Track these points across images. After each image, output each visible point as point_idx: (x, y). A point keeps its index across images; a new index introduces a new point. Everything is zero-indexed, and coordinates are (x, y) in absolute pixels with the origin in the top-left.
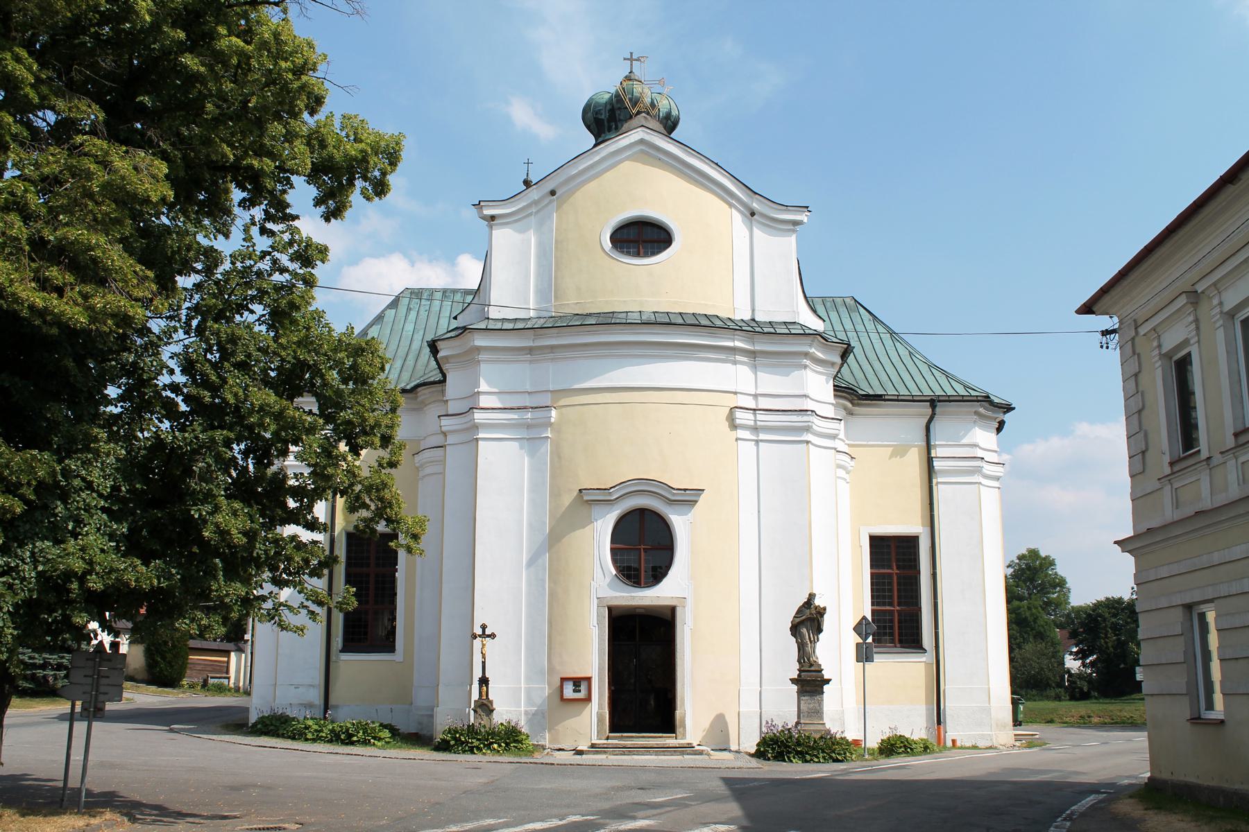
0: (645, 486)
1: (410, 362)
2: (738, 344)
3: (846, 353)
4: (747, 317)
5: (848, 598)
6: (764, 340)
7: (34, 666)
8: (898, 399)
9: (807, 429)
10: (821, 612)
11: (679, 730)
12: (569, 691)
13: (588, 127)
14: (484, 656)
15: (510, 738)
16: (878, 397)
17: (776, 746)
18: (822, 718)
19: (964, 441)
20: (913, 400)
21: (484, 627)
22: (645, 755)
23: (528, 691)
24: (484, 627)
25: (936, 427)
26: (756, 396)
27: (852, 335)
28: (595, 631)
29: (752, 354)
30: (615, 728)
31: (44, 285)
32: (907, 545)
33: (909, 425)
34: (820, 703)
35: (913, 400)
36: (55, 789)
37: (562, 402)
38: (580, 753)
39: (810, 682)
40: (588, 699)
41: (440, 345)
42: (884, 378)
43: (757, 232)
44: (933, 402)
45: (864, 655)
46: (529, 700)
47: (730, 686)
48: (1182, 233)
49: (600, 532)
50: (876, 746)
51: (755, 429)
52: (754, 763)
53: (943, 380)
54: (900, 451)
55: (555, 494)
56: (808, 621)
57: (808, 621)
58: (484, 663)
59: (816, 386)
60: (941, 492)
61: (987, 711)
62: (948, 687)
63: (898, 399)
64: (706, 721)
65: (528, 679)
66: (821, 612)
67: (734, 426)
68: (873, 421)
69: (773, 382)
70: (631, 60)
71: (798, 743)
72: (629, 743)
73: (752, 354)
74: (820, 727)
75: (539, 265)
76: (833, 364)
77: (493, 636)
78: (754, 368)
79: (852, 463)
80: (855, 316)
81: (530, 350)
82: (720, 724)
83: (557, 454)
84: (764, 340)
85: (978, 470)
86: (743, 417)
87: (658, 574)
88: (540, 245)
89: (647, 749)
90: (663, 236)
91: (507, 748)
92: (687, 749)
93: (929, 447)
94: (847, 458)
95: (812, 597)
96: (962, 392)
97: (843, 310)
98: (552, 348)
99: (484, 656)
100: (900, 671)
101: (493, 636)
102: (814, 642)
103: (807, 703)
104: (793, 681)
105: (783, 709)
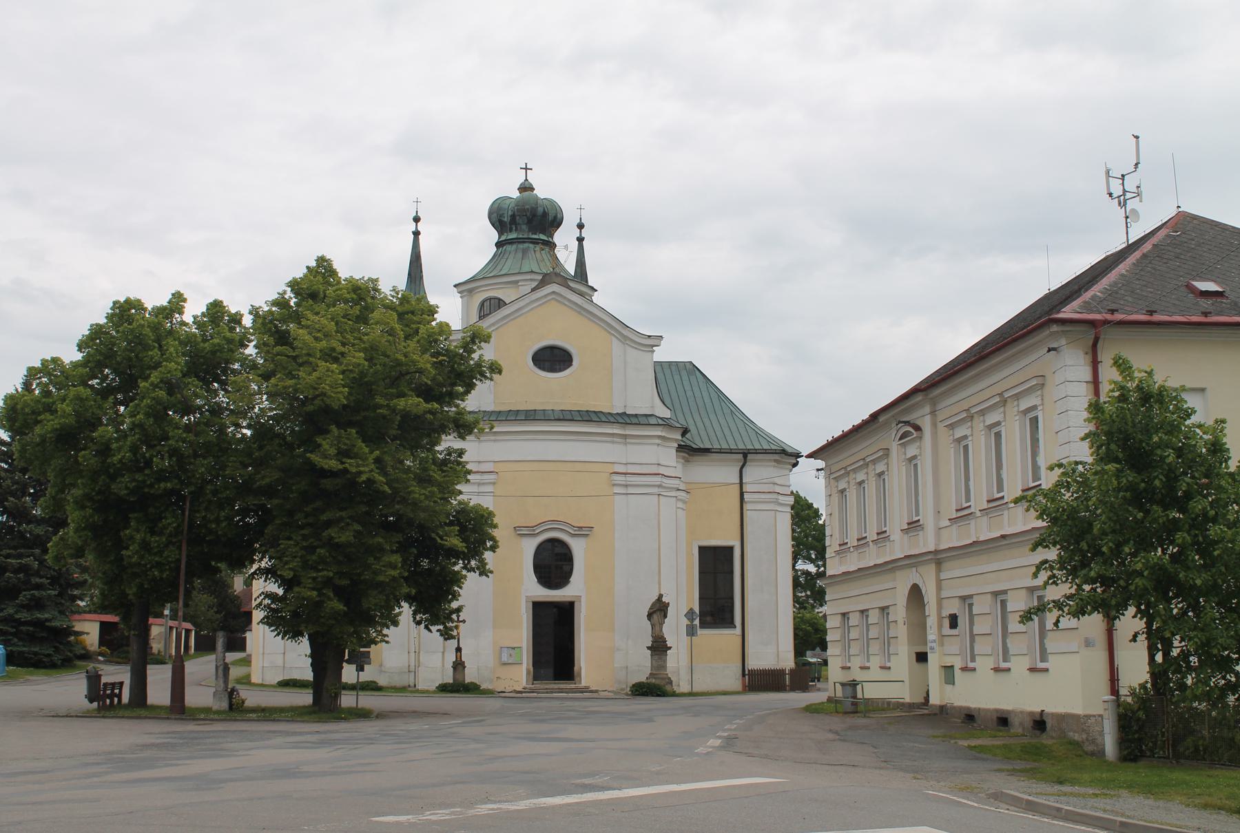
0: (555, 524)
2: (616, 431)
3: (685, 432)
5: (684, 594)
8: (720, 451)
11: (577, 679)
16: (707, 451)
20: (731, 452)
25: (746, 470)
27: (691, 422)
34: (665, 661)
35: (731, 452)
39: (659, 647)
43: (630, 350)
45: (691, 632)
47: (607, 649)
56: (659, 609)
57: (659, 609)
59: (667, 457)
62: (749, 651)
63: (720, 451)
70: (526, 169)
72: (562, 686)
77: (464, 621)
80: (693, 378)
89: (561, 691)
94: (683, 494)
95: (661, 596)
97: (684, 373)
100: (721, 639)
102: (661, 624)
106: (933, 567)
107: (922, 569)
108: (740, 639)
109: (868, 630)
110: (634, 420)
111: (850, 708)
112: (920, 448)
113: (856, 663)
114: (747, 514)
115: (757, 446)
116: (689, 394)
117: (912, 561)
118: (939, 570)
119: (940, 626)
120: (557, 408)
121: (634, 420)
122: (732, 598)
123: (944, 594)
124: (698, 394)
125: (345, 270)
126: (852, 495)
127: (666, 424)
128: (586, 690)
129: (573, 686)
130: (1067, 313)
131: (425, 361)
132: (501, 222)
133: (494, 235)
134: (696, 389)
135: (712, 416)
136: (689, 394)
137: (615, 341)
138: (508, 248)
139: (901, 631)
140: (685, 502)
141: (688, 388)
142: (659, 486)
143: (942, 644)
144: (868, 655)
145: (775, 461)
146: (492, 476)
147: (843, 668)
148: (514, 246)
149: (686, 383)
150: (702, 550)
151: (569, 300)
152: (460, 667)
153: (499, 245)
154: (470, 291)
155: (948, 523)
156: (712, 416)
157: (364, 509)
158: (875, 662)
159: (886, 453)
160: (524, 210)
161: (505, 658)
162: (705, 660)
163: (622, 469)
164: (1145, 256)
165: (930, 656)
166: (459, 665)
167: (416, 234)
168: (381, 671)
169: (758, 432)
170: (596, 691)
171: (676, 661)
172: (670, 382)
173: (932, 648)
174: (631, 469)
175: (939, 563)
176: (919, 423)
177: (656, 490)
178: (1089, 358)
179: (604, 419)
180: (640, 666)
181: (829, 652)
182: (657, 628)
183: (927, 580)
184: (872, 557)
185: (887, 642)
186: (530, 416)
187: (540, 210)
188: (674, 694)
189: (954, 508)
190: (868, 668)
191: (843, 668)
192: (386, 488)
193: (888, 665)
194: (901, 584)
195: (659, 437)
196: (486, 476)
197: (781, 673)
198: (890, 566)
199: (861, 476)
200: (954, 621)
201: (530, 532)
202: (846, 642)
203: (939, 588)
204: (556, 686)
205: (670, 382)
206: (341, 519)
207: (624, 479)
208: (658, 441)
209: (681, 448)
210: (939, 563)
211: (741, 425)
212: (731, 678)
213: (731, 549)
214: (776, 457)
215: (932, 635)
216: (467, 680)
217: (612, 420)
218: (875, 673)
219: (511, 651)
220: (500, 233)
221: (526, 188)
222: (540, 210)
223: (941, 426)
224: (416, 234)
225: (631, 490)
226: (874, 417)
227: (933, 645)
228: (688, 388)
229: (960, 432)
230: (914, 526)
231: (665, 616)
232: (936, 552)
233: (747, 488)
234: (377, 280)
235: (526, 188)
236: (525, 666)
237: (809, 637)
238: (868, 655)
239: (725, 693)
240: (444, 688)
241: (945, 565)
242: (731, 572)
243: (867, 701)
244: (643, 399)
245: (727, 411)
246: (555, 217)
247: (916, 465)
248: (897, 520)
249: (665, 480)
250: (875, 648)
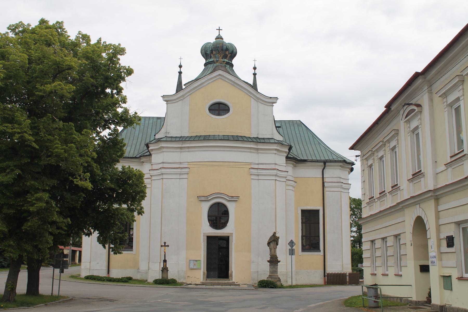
1: (138, 147)
2: (252, 146)
3: (290, 148)
5: (292, 231)
11: (230, 278)
13: (203, 56)
14: (165, 253)
16: (305, 161)
18: (277, 274)
20: (317, 161)
21: (165, 243)
24: (165, 243)
28: (203, 244)
30: (208, 277)
34: (277, 268)
35: (317, 161)
36: (49, 296)
39: (274, 261)
41: (150, 145)
42: (308, 152)
43: (260, 104)
44: (325, 162)
45: (292, 252)
47: (246, 263)
48: (381, 125)
50: (83, 277)
53: (329, 154)
58: (165, 255)
59: (281, 160)
70: (219, 30)
74: (276, 277)
76: (286, 152)
77: (168, 246)
79: (296, 184)
80: (300, 128)
81: (181, 148)
87: (223, 225)
89: (219, 284)
90: (227, 108)
94: (293, 183)
95: (275, 233)
98: (188, 147)
99: (165, 253)
100: (316, 256)
101: (168, 246)
102: (275, 248)
104: (268, 261)
106: (432, 202)
107: (424, 205)
108: (323, 257)
109: (387, 251)
110: (262, 141)
111: (373, 304)
112: (420, 119)
113: (380, 271)
114: (326, 193)
115: (331, 158)
116: (298, 135)
117: (416, 200)
118: (437, 204)
119: (439, 246)
120: (221, 134)
121: (262, 141)
122: (319, 236)
123: (441, 222)
124: (302, 135)
126: (376, 167)
127: (279, 143)
128: (233, 284)
129: (226, 282)
131: (75, 62)
132: (206, 54)
133: (203, 61)
135: (309, 145)
136: (298, 135)
137: (252, 100)
138: (209, 66)
139: (409, 250)
140: (294, 187)
141: (297, 132)
142: (276, 175)
143: (441, 259)
144: (387, 267)
145: (341, 166)
146: (187, 170)
147: (383, 275)
148: (212, 65)
149: (297, 130)
150: (303, 211)
151: (228, 79)
152: (165, 271)
153: (206, 65)
155: (444, 168)
156: (309, 145)
157: (28, 160)
158: (391, 271)
159: (397, 132)
160: (217, 47)
161: (192, 266)
162: (298, 268)
163: (256, 166)
165: (431, 268)
166: (165, 270)
167: (180, 73)
168: (138, 272)
169: (332, 152)
170: (239, 285)
171: (282, 269)
172: (289, 130)
173: (433, 262)
174: (261, 166)
175: (437, 199)
176: (419, 103)
177: (274, 178)
179: (245, 140)
180: (264, 271)
181: (364, 264)
182: (273, 251)
183: (428, 212)
184: (389, 202)
185: (400, 258)
186: (206, 138)
187: (225, 47)
188: (282, 287)
189: (449, 155)
190: (387, 275)
191: (383, 275)
192: (34, 145)
193: (400, 273)
194: (409, 218)
195: (276, 150)
196: (184, 170)
197: (344, 275)
198: (401, 206)
199: (381, 154)
200: (450, 242)
201: (202, 199)
202: (373, 259)
203: (438, 217)
204: (217, 282)
205: (289, 130)
206: (8, 167)
207: (256, 171)
208: (275, 152)
209: (287, 158)
210: (437, 199)
211: (323, 149)
212: (318, 278)
213: (318, 211)
214: (341, 164)
215: (433, 252)
216: (169, 278)
217: (250, 140)
218: (392, 279)
219: (195, 262)
221: (219, 38)
222: (225, 47)
223: (436, 98)
224: (180, 73)
225: (260, 177)
226: (388, 106)
227: (433, 259)
228: (297, 132)
229: (451, 98)
231: (277, 244)
232: (435, 190)
233: (326, 180)
234: (62, 22)
235: (219, 38)
236: (202, 270)
237: (357, 258)
238: (387, 267)
239: (311, 286)
240: (157, 282)
241: (441, 201)
242: (318, 223)
243: (387, 298)
244: (268, 131)
245: (316, 142)
246: (233, 52)
247: (418, 135)
248: (406, 172)
249: (279, 172)
250: (391, 262)
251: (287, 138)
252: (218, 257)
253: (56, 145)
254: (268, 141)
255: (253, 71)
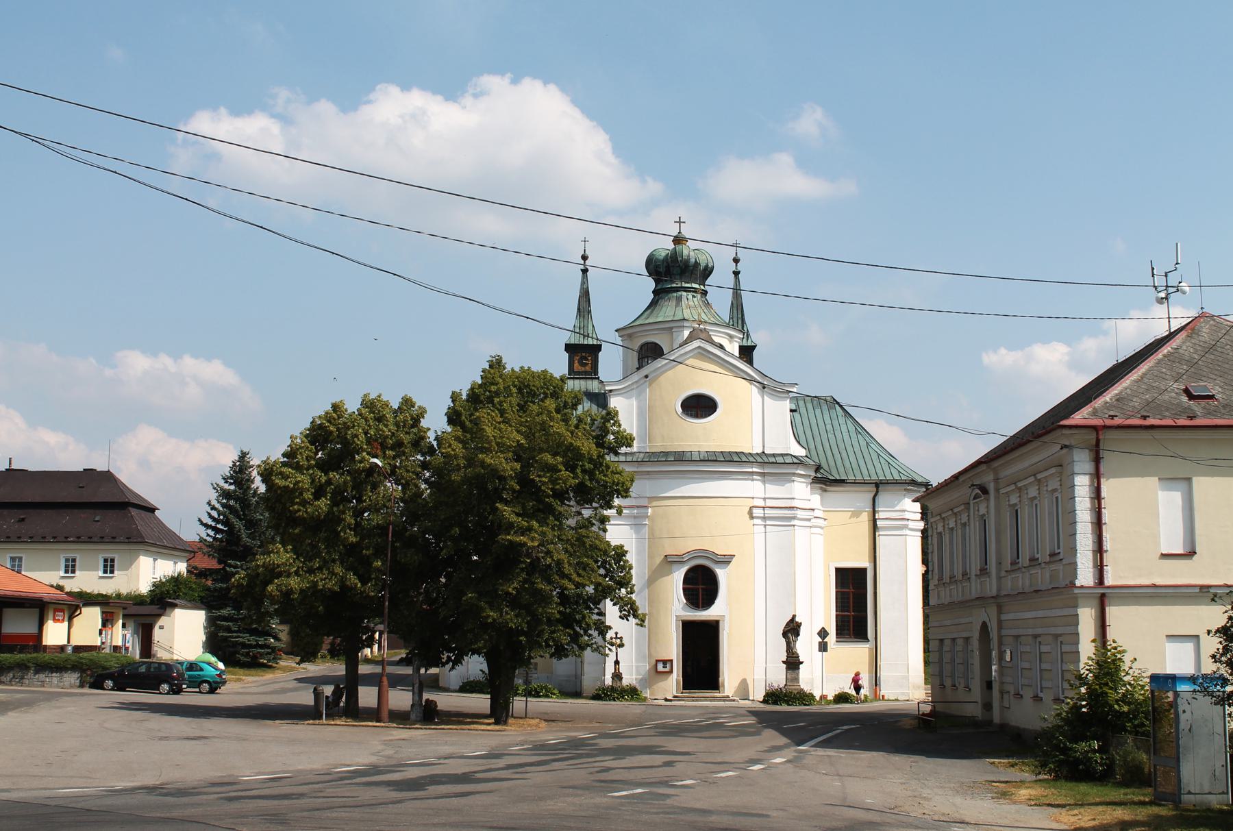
0: (702, 554)
2: (755, 470)
4: (760, 451)
5: (818, 609)
6: (770, 466)
7: (251, 646)
9: (794, 518)
10: (799, 625)
12: (660, 667)
15: (632, 693)
16: (842, 481)
17: (773, 696)
19: (897, 508)
22: (703, 701)
23: (637, 667)
25: (880, 499)
26: (765, 499)
28: (674, 635)
29: (763, 475)
31: (579, 575)
32: (862, 572)
33: (862, 498)
37: (654, 504)
38: (666, 700)
39: (793, 663)
40: (671, 671)
45: (823, 647)
46: (638, 672)
47: (749, 665)
49: (677, 578)
51: (764, 518)
52: (762, 705)
54: (856, 514)
55: (651, 557)
56: (792, 629)
57: (792, 629)
60: (881, 541)
61: (907, 678)
62: (882, 662)
64: (736, 683)
65: (637, 661)
66: (799, 625)
67: (752, 517)
68: (838, 496)
69: (775, 491)
70: (680, 222)
71: (785, 695)
73: (763, 475)
75: (639, 420)
78: (764, 482)
82: (744, 684)
83: (652, 537)
84: (770, 466)
85: (906, 527)
86: (757, 512)
88: (639, 408)
89: (706, 699)
91: (632, 699)
92: (726, 698)
93: (874, 512)
95: (794, 616)
96: (896, 477)
100: (854, 655)
103: (791, 674)
105: (778, 677)
115: (889, 477)
116: (829, 427)
121: (772, 460)
123: (1004, 632)
125: (513, 364)
127: (799, 462)
130: (1078, 418)
133: (651, 284)
134: (835, 423)
136: (829, 427)
141: (828, 421)
150: (838, 570)
154: (630, 336)
164: (1160, 361)
178: (1093, 455)
179: (744, 459)
220: (657, 282)
226: (956, 477)
228: (828, 421)
230: (984, 571)
251: (813, 452)
252: (701, 653)
253: (591, 562)
254: (780, 460)
255: (733, 267)
